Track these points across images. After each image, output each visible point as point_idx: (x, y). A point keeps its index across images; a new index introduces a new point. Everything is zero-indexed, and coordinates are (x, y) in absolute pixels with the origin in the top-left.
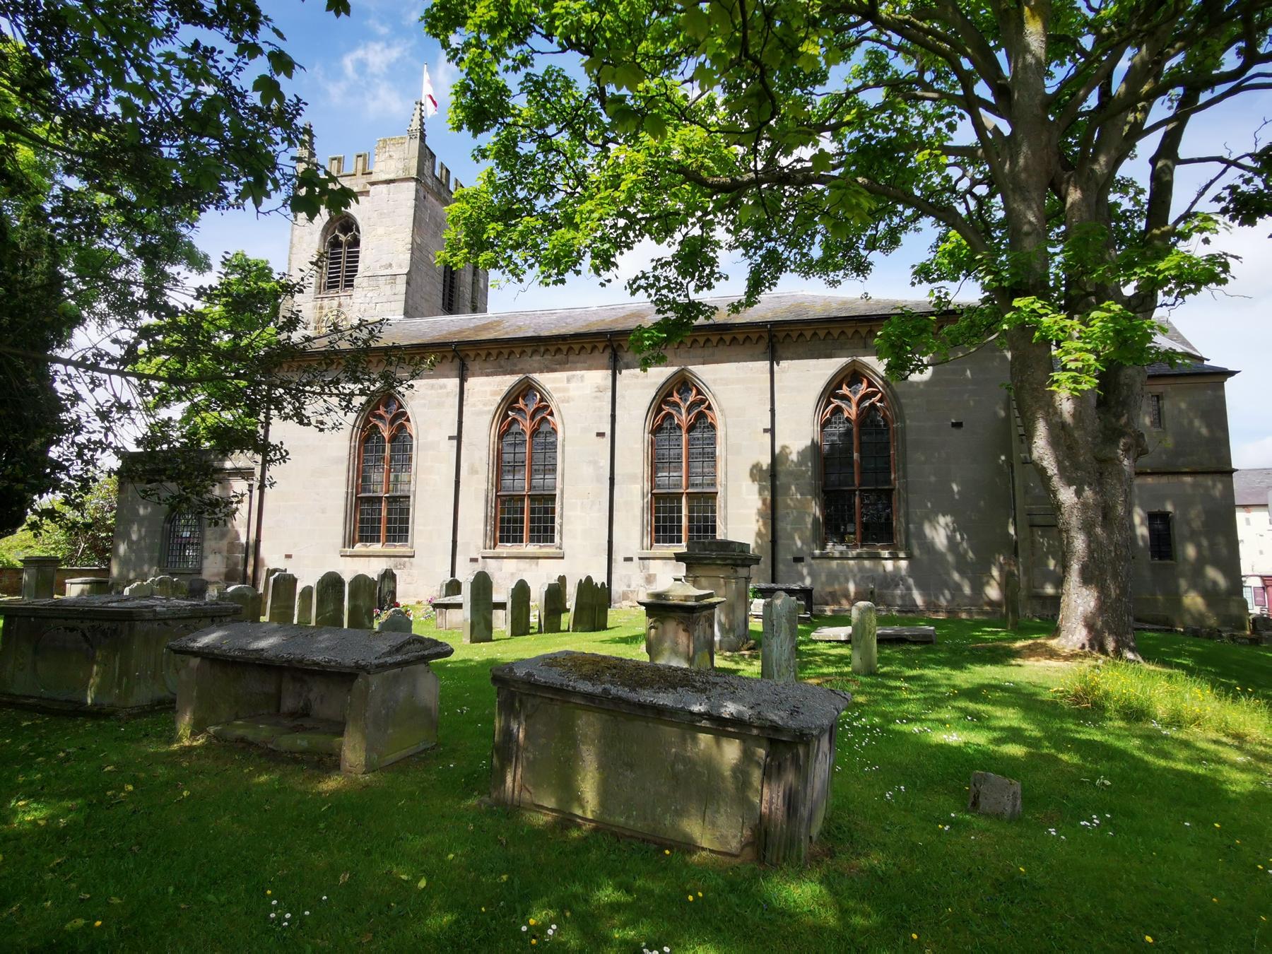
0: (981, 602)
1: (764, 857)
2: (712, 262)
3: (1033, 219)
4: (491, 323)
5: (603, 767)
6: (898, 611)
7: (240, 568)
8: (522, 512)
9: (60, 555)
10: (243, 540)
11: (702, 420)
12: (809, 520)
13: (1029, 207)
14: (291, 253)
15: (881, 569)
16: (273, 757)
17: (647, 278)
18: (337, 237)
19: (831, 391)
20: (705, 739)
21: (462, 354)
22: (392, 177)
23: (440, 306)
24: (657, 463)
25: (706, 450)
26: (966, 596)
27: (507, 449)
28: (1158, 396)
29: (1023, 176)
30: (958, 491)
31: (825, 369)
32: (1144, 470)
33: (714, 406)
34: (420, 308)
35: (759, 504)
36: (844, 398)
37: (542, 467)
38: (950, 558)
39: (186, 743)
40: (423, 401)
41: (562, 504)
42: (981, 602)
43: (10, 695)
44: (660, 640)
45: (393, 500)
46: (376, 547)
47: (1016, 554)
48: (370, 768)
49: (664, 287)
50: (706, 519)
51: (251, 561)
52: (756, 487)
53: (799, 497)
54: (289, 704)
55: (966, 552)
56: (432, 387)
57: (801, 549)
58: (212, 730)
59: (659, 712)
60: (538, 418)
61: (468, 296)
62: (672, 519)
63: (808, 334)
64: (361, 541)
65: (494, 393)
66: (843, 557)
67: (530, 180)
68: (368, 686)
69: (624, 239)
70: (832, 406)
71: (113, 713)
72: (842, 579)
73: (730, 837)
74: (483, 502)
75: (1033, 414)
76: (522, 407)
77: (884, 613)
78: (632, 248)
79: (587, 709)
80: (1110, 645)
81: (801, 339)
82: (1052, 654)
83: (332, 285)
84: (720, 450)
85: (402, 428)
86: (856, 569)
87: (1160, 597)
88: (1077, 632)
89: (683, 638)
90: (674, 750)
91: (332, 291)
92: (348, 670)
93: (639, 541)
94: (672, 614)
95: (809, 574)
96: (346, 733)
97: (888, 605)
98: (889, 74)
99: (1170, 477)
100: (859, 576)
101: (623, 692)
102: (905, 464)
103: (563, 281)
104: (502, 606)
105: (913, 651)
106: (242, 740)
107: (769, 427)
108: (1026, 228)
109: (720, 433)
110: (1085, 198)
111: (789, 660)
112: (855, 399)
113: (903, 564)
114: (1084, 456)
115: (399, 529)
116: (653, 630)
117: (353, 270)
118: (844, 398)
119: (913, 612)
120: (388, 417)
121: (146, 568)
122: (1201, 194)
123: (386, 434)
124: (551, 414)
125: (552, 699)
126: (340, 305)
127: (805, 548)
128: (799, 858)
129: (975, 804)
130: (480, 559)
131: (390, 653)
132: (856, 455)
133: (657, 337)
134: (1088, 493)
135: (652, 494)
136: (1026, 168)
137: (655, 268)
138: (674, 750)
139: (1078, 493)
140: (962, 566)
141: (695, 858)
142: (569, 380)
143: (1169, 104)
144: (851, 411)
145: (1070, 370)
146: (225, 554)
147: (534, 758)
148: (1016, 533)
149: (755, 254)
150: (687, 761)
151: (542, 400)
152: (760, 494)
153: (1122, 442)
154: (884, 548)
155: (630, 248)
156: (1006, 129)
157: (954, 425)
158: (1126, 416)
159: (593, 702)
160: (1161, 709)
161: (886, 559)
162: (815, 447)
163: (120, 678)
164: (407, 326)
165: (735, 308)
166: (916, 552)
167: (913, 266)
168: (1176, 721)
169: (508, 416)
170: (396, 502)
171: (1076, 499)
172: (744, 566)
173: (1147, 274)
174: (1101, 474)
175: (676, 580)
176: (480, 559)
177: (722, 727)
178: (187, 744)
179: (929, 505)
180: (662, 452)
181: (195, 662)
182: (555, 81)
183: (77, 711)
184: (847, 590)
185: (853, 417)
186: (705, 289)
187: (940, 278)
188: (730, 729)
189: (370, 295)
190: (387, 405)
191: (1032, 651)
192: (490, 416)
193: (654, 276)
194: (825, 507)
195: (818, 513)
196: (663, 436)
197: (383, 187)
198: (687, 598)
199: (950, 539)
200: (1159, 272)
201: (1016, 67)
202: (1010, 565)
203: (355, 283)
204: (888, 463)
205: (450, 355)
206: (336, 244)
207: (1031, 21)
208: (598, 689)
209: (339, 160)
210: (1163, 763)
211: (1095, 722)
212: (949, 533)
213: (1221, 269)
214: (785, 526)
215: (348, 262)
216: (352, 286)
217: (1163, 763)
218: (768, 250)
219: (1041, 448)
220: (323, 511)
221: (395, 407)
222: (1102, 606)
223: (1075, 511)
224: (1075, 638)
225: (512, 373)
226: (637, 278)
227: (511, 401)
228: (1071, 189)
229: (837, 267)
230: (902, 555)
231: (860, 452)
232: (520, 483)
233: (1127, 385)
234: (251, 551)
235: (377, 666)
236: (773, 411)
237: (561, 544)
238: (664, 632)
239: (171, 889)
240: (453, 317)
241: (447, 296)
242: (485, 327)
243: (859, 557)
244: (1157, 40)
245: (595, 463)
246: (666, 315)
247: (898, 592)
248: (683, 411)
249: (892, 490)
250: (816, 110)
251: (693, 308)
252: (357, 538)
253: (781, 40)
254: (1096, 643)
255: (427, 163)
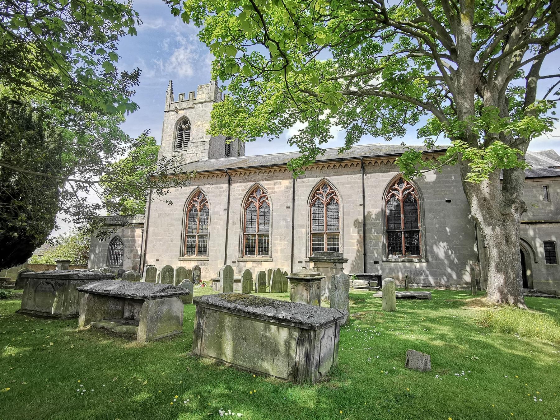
0: (462, 282)
1: (297, 380)
2: (327, 131)
3: (468, 106)
4: (244, 161)
5: (234, 340)
6: (422, 286)
7: (138, 265)
8: (255, 242)
9: (71, 260)
10: (139, 253)
11: (332, 200)
12: (381, 245)
13: (466, 101)
14: (163, 134)
15: (414, 267)
16: (112, 334)
17: (297, 138)
18: (181, 126)
19: (390, 187)
20: (273, 328)
21: (229, 174)
22: (204, 100)
23: (224, 154)
24: (312, 219)
25: (334, 214)
26: (455, 280)
27: (248, 214)
28: (546, 187)
29: (463, 87)
30: (450, 232)
31: (387, 177)
32: (540, 221)
33: (338, 194)
34: (215, 155)
35: (358, 237)
36: (396, 190)
37: (263, 222)
38: (446, 262)
39: (82, 328)
40: (213, 194)
41: (272, 238)
42: (462, 282)
43: (26, 310)
44: (295, 294)
45: (202, 236)
46: (194, 256)
47: (478, 260)
48: (148, 340)
49: (305, 142)
50: (335, 245)
51: (142, 262)
52: (356, 230)
53: (376, 234)
54: (127, 314)
55: (454, 259)
56: (217, 188)
57: (377, 257)
58: (92, 323)
59: (255, 316)
60: (262, 201)
61: (236, 150)
62: (320, 245)
63: (379, 162)
64: (187, 254)
65: (243, 190)
66: (396, 262)
67: (248, 99)
68: (148, 305)
69: (288, 122)
70: (391, 194)
71: (60, 317)
72: (396, 271)
73: (283, 371)
74: (238, 238)
75: (471, 194)
76: (255, 196)
77: (416, 287)
78: (292, 126)
79: (228, 314)
80: (511, 300)
81: (376, 164)
82: (482, 304)
83: (179, 146)
84: (340, 214)
85: (205, 205)
86: (402, 267)
87: (551, 282)
88: (495, 294)
89: (305, 293)
90: (262, 333)
91: (179, 149)
92: (141, 298)
93: (305, 254)
94: (300, 283)
95: (381, 269)
96: (139, 325)
97: (418, 284)
98: (411, 46)
99: (554, 224)
100: (404, 270)
101: (243, 307)
102: (424, 219)
103: (255, 140)
104: (238, 281)
105: (418, 302)
106: (103, 328)
107: (362, 203)
108: (464, 111)
109: (341, 206)
110: (492, 96)
111: (345, 302)
112: (401, 190)
113: (424, 265)
114: (496, 213)
115: (203, 249)
116: (293, 290)
117: (187, 140)
118: (396, 190)
119: (429, 287)
120: (199, 201)
121: (101, 265)
122: (550, 91)
123: (198, 208)
124: (267, 199)
125: (216, 311)
126: (182, 155)
127: (379, 257)
128: (311, 381)
129: (407, 364)
130: (237, 262)
131: (159, 292)
132: (402, 216)
133: (299, 163)
134: (498, 229)
135: (311, 233)
136: (464, 84)
137: (301, 134)
138: (262, 333)
139: (493, 229)
140: (452, 265)
141: (268, 379)
142: (274, 184)
143: (535, 52)
144: (399, 196)
145: (476, 172)
146: (132, 259)
147: (209, 335)
148: (478, 249)
149: (347, 126)
150: (266, 337)
151: (263, 193)
152: (358, 233)
153: (513, 206)
154: (415, 257)
155: (291, 126)
156: (455, 66)
157: (447, 201)
158: (516, 194)
159: (231, 311)
160: (521, 329)
161: (416, 262)
162: (383, 212)
163: (64, 303)
164: (209, 163)
165: (341, 151)
166: (430, 259)
167: (418, 130)
168: (528, 334)
169: (249, 200)
170: (202, 237)
171: (492, 233)
172: (339, 263)
173: (514, 128)
174: (504, 221)
175: (303, 268)
176: (237, 262)
177: (280, 322)
178: (82, 329)
179: (436, 238)
180: (315, 215)
181: (87, 295)
182: (256, 57)
183: (48, 316)
184: (398, 276)
185: (400, 198)
186: (324, 142)
187: (431, 134)
188: (283, 323)
189: (194, 150)
190: (198, 196)
191: (473, 303)
192: (241, 201)
193: (300, 137)
194: (389, 239)
195: (385, 242)
196: (316, 208)
197: (200, 105)
198: (306, 275)
199: (446, 253)
200: (519, 127)
201: (458, 40)
202: (475, 265)
203: (188, 145)
204: (417, 219)
205: (225, 174)
206: (181, 129)
207: (464, 19)
208: (232, 306)
209: (183, 95)
210: (510, 351)
211: (485, 333)
212: (446, 251)
213: (549, 125)
214: (369, 247)
215: (186, 137)
216: (187, 146)
217: (510, 351)
218: (354, 125)
219: (476, 211)
220: (172, 241)
221: (202, 197)
222: (507, 283)
223: (492, 238)
224: (494, 297)
225: (251, 181)
226: (292, 138)
227: (251, 193)
228: (485, 92)
229: (389, 132)
230: (423, 260)
231: (404, 214)
232: (254, 229)
233: (516, 179)
234: (142, 258)
235: (152, 297)
236: (364, 196)
237: (271, 255)
238: (297, 290)
239: (47, 380)
240: (229, 159)
241: (227, 150)
242: (241, 163)
243: (403, 261)
244: (522, 24)
245: (286, 220)
246: (304, 154)
247: (422, 277)
248: (324, 197)
249: (419, 231)
250: (378, 64)
251: (315, 151)
252: (185, 252)
253: (305, 33)
254: (504, 299)
255: (218, 94)
